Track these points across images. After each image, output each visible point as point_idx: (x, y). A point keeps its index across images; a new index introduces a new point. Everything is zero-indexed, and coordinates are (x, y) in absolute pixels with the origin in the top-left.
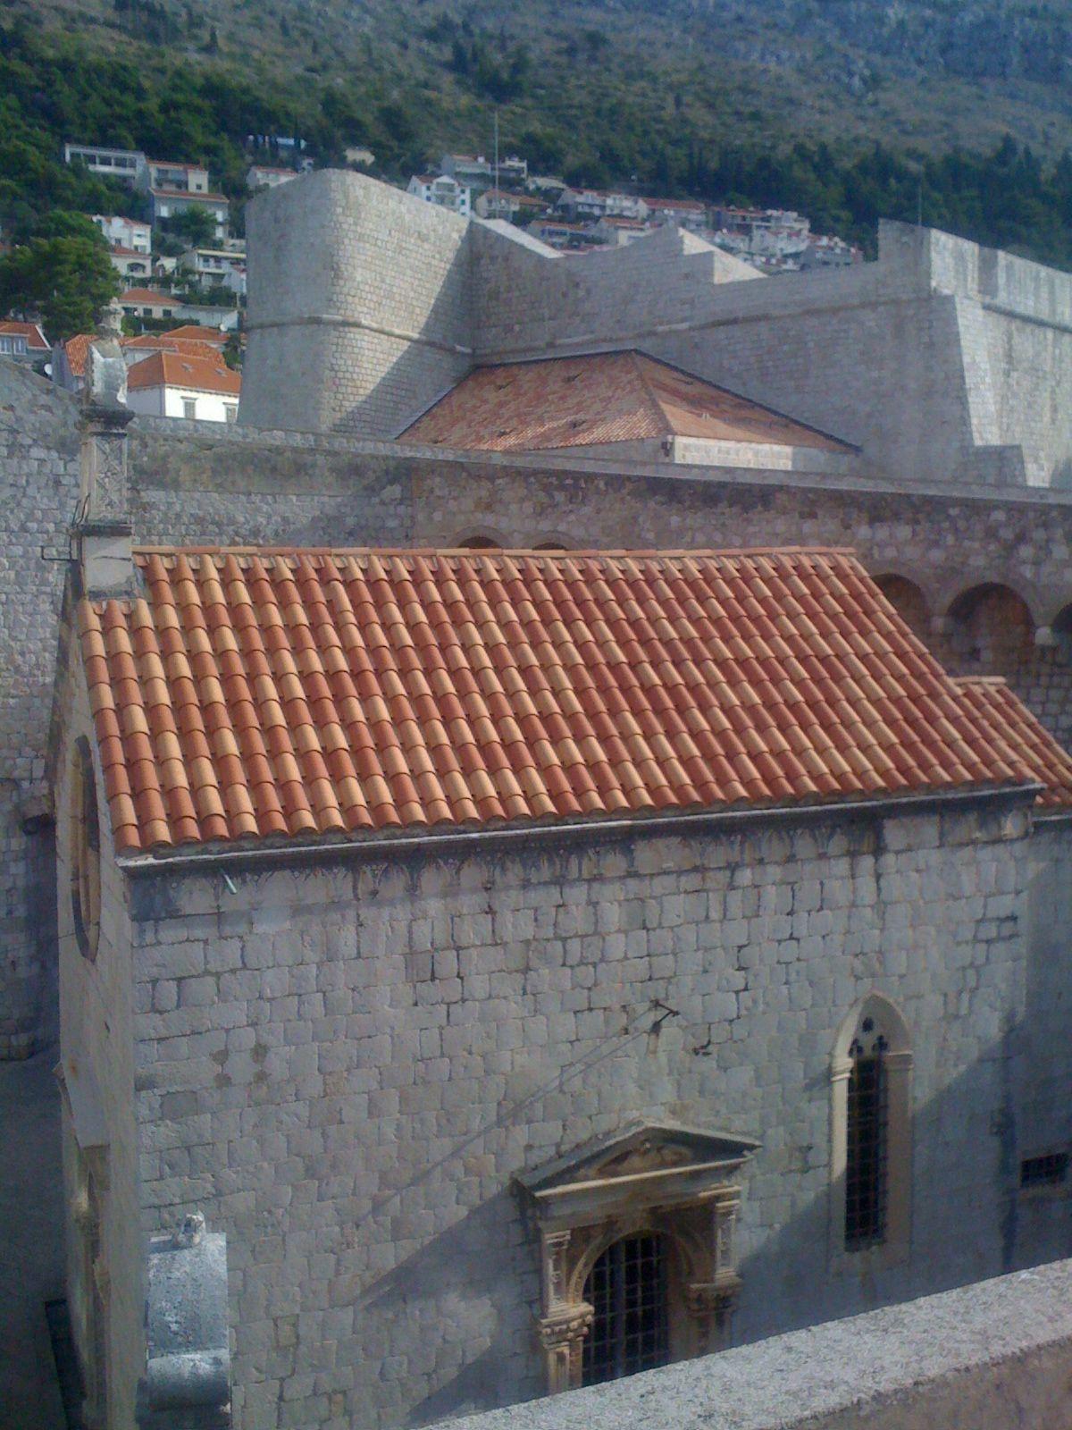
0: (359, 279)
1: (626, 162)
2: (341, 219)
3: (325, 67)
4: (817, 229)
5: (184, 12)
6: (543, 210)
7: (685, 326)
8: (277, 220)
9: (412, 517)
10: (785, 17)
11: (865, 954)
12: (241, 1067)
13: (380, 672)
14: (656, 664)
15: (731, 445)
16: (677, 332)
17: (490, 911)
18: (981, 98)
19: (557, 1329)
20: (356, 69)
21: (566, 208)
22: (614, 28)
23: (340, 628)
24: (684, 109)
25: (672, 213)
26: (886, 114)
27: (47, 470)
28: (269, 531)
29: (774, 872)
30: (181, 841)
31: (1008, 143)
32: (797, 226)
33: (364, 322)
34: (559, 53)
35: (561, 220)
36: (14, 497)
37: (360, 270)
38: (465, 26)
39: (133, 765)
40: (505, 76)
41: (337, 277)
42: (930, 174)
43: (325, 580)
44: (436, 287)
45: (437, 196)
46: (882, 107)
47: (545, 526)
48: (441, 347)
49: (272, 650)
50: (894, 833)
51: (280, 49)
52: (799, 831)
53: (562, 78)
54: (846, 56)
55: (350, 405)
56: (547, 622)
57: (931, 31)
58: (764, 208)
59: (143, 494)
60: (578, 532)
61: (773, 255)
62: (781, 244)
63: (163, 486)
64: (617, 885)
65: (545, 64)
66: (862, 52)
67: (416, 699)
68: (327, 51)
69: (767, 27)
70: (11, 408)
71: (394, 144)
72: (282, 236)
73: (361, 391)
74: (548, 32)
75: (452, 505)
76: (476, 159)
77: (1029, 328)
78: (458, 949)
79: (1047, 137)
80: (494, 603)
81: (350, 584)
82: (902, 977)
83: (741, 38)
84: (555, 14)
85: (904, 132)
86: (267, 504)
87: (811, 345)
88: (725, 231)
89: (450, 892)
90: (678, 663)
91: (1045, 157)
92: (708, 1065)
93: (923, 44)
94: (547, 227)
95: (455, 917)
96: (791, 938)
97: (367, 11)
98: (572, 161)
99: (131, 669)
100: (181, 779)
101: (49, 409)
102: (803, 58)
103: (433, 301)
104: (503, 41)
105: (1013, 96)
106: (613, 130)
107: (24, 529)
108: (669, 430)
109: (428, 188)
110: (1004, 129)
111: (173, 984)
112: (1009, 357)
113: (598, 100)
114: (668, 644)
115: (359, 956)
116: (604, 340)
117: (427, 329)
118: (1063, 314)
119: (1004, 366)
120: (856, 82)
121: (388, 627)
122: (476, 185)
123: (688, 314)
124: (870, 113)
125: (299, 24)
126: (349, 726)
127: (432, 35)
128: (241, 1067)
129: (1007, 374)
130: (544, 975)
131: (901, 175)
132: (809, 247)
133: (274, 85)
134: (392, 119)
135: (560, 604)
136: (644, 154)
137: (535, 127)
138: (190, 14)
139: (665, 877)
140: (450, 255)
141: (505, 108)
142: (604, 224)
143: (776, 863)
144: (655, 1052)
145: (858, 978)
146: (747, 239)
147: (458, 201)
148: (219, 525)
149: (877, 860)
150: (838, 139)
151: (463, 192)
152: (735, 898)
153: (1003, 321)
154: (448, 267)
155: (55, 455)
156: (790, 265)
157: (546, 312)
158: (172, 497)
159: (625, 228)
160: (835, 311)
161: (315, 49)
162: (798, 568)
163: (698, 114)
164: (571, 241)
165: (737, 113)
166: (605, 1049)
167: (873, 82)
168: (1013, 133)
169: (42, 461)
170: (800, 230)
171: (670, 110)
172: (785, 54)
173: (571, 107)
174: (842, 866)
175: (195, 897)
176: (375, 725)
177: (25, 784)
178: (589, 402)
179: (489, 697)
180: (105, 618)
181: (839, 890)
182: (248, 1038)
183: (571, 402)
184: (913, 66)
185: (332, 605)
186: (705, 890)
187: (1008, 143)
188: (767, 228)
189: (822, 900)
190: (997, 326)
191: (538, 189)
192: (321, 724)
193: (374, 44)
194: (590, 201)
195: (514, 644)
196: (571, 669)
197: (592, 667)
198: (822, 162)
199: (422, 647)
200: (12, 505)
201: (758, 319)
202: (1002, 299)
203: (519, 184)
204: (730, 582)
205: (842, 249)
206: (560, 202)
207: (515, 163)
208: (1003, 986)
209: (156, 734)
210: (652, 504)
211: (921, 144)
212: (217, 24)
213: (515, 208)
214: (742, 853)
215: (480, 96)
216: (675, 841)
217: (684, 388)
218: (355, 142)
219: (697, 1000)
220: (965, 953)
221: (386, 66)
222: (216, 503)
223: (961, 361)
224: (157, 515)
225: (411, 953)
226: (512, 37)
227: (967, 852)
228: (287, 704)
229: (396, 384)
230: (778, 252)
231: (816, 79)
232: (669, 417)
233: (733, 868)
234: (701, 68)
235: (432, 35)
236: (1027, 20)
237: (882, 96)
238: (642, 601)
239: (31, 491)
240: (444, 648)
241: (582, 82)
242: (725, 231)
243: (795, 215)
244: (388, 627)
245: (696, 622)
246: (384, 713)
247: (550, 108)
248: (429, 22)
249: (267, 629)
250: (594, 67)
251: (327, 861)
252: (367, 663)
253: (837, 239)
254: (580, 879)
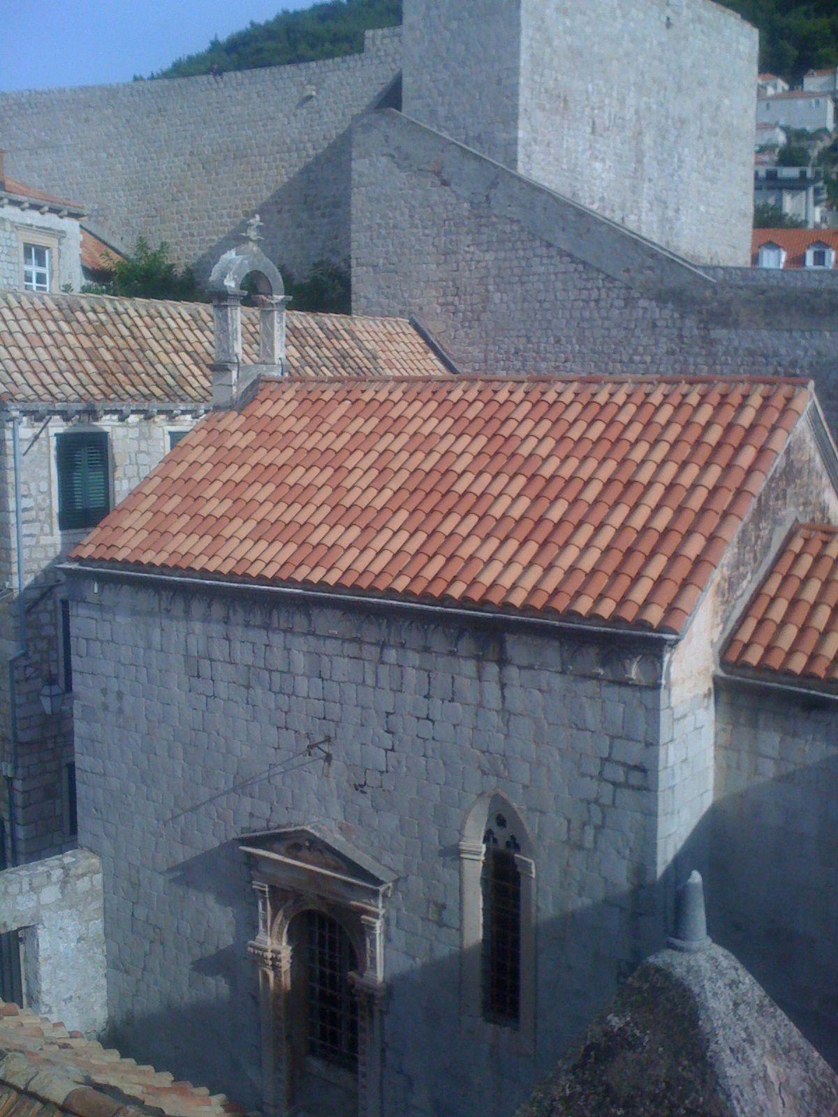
11: (490, 753)
17: (227, 639)
19: (256, 951)
27: (648, 316)
28: (806, 363)
29: (414, 658)
36: (626, 337)
50: (517, 649)
52: (432, 626)
59: (712, 332)
64: (302, 640)
70: (628, 271)
78: (211, 660)
82: (525, 787)
86: (806, 339)
89: (206, 619)
92: (364, 801)
96: (428, 718)
101: (651, 268)
107: (631, 361)
115: (162, 651)
130: (258, 693)
139: (334, 641)
143: (414, 650)
144: (327, 776)
145: (484, 773)
148: (766, 356)
149: (501, 669)
152: (384, 671)
155: (654, 304)
166: (295, 762)
169: (645, 309)
174: (469, 667)
181: (466, 686)
186: (361, 659)
189: (453, 693)
200: (625, 343)
208: (632, 836)
214: (389, 634)
216: (339, 613)
219: (357, 747)
220: (591, 788)
222: (767, 338)
227: (591, 686)
233: (383, 645)
239: (638, 332)
254: (278, 629)
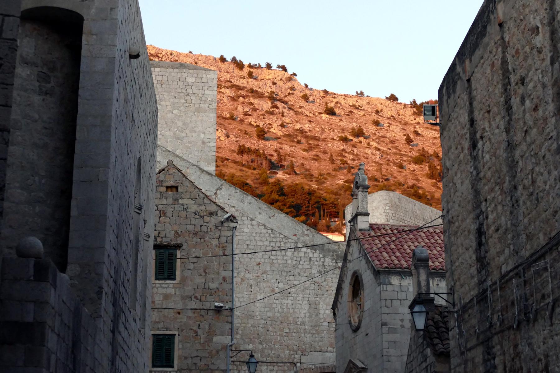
5: (275, 154)
70: (295, 235)
111: (390, 301)
138: (279, 155)
169: (305, 253)
177: (298, 365)
212: (293, 159)
248: (414, 154)
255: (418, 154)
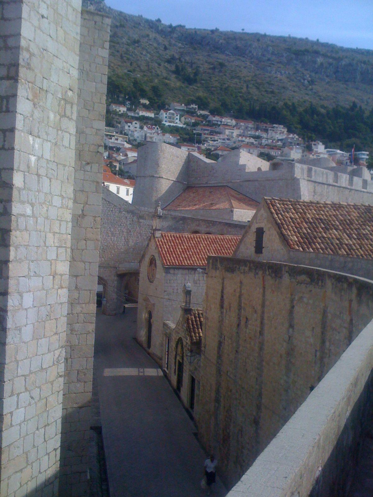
0: (163, 167)
1: (229, 107)
2: (160, 153)
3: (134, 70)
4: (290, 131)
6: (202, 122)
7: (238, 181)
8: (145, 153)
9: (184, 227)
10: (285, 60)
12: (175, 291)
13: (190, 249)
14: (224, 250)
15: (247, 211)
16: (237, 182)
17: (203, 276)
18: (347, 89)
20: (144, 72)
21: (209, 121)
22: (228, 61)
23: (185, 243)
24: (249, 89)
25: (243, 124)
26: (315, 93)
30: (171, 265)
31: (355, 105)
32: (283, 130)
33: (164, 177)
34: (209, 69)
35: (208, 125)
37: (163, 165)
38: (179, 59)
39: (164, 257)
40: (192, 76)
41: (159, 166)
42: (328, 113)
43: (183, 238)
44: (180, 168)
45: (169, 117)
46: (314, 91)
47: (208, 229)
48: (180, 182)
49: (178, 246)
51: (120, 63)
53: (210, 77)
54: (303, 73)
55: (159, 196)
56: (211, 244)
57: (331, 66)
58: (273, 123)
60: (214, 231)
61: (274, 140)
62: (277, 136)
63: (143, 219)
65: (205, 72)
66: (309, 72)
67: (195, 252)
68: (134, 65)
69: (278, 63)
70: (120, 205)
71: (155, 98)
72: (146, 157)
73: (162, 193)
74: (206, 62)
75: (192, 225)
76: (181, 105)
77: (320, 185)
79: (367, 102)
80: (204, 241)
81: (186, 238)
83: (270, 66)
84: (209, 55)
85: (320, 99)
87: (267, 188)
88: (260, 131)
90: (227, 250)
91: (366, 109)
93: (329, 70)
94: (203, 128)
95: (199, 277)
97: (148, 52)
98: (212, 105)
99: (162, 247)
100: (170, 259)
102: (289, 73)
103: (179, 172)
104: (192, 64)
105: (357, 89)
106: (226, 95)
107: (121, 225)
108: (233, 207)
109: (166, 114)
110: (353, 99)
112: (314, 192)
113: (222, 85)
114: (226, 247)
116: (220, 183)
117: (177, 178)
118: (330, 181)
119: (313, 194)
120: (306, 82)
121: (191, 244)
122: (181, 113)
123: (239, 178)
124: (310, 93)
125: (126, 55)
126: (187, 255)
127: (169, 61)
128: (175, 291)
129: (314, 196)
131: (318, 114)
132: (286, 138)
133: (118, 76)
134: (155, 89)
135: (212, 242)
136: (235, 103)
137: (201, 94)
140: (184, 161)
141: (191, 87)
142: (221, 127)
146: (267, 134)
147: (175, 119)
150: (299, 101)
151: (177, 116)
153: (313, 183)
154: (183, 163)
156: (280, 143)
157: (206, 175)
158: (144, 221)
159: (228, 129)
160: (273, 180)
161: (131, 64)
162: (173, 236)
163: (254, 91)
164: (210, 133)
165: (266, 91)
167: (312, 82)
168: (356, 101)
169: (124, 214)
170: (284, 132)
171: (244, 90)
172: (283, 72)
173: (212, 87)
175: (172, 271)
176: (190, 255)
177: (118, 268)
178: (215, 198)
179: (203, 253)
180: (158, 240)
182: (176, 288)
183: (211, 198)
184: (325, 77)
185: (184, 240)
187: (355, 105)
188: (273, 130)
190: (311, 186)
191: (201, 114)
192: (184, 254)
193: (150, 64)
194: (217, 120)
195: (206, 246)
196: (213, 250)
197: (216, 250)
198: (292, 109)
199: (195, 246)
201: (255, 181)
202: (313, 178)
203: (195, 113)
204: (235, 240)
205: (297, 139)
206: (207, 120)
207: (194, 106)
209: (166, 254)
210: (226, 227)
211: (326, 103)
213: (193, 121)
215: (183, 83)
217: (237, 196)
218: (143, 97)
221: (154, 71)
223: (300, 194)
224: (142, 224)
225: (194, 280)
226: (194, 63)
228: (180, 252)
229: (170, 191)
230: (276, 139)
231: (293, 81)
232: (233, 204)
234: (255, 75)
235: (169, 61)
236: (363, 65)
237: (314, 87)
238: (223, 242)
240: (198, 246)
241: (217, 79)
242: (260, 131)
243: (282, 126)
244: (191, 244)
245: (230, 245)
246: (191, 254)
247: (206, 88)
248: (168, 57)
249: (176, 243)
250: (221, 74)
251: (186, 269)
252: (189, 248)
253: (295, 135)
255: (170, 58)
